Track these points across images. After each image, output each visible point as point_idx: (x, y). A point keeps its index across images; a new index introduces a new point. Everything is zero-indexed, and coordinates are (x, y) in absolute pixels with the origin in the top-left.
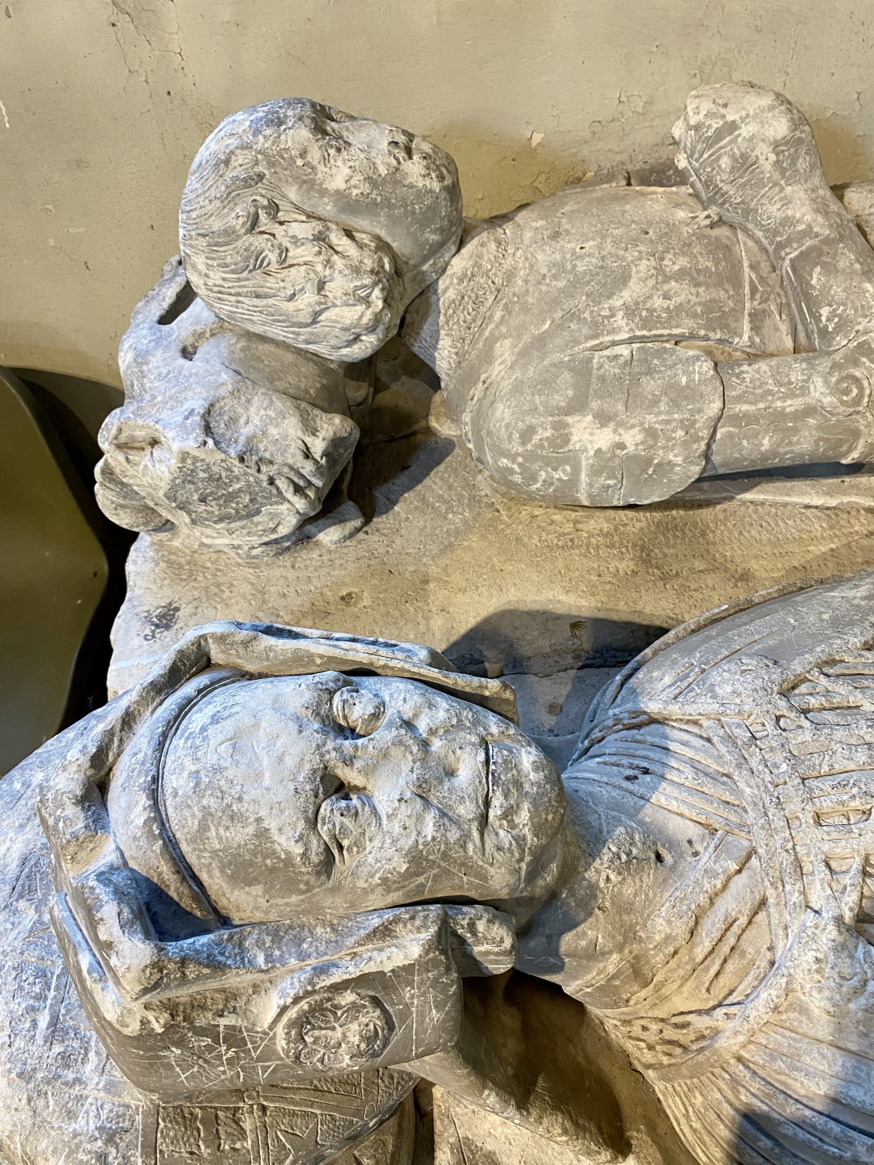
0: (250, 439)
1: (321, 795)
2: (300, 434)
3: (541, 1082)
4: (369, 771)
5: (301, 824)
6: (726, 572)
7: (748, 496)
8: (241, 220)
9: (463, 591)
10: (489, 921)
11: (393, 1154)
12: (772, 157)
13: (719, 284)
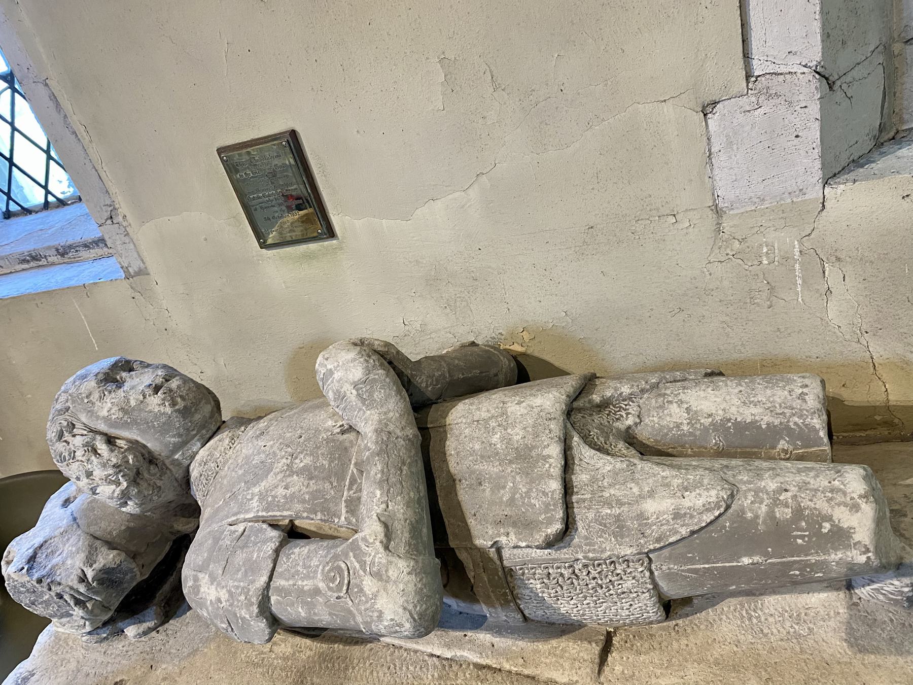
0: (53, 567)
2: (81, 565)
8: (54, 434)
12: (354, 392)
13: (327, 478)
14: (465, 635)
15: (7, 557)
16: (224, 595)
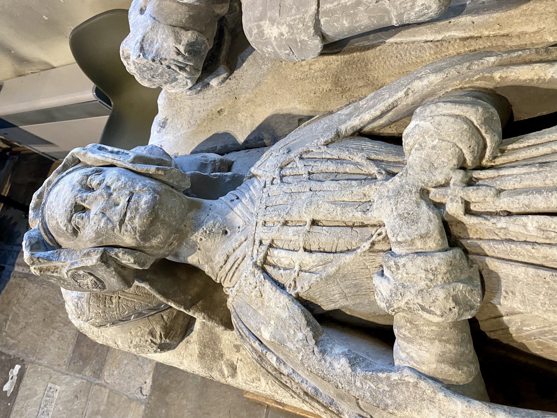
1: (73, 212)
2: (174, 44)
3: (200, 302)
4: (90, 204)
5: (66, 221)
6: (373, 86)
7: (392, 40)
9: (260, 105)
10: (123, 254)
11: (175, 316)
14: (450, 22)
15: (123, 55)
16: (284, 29)
